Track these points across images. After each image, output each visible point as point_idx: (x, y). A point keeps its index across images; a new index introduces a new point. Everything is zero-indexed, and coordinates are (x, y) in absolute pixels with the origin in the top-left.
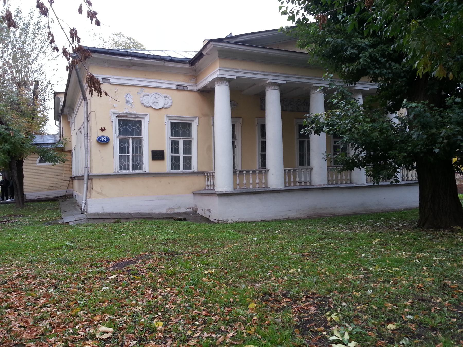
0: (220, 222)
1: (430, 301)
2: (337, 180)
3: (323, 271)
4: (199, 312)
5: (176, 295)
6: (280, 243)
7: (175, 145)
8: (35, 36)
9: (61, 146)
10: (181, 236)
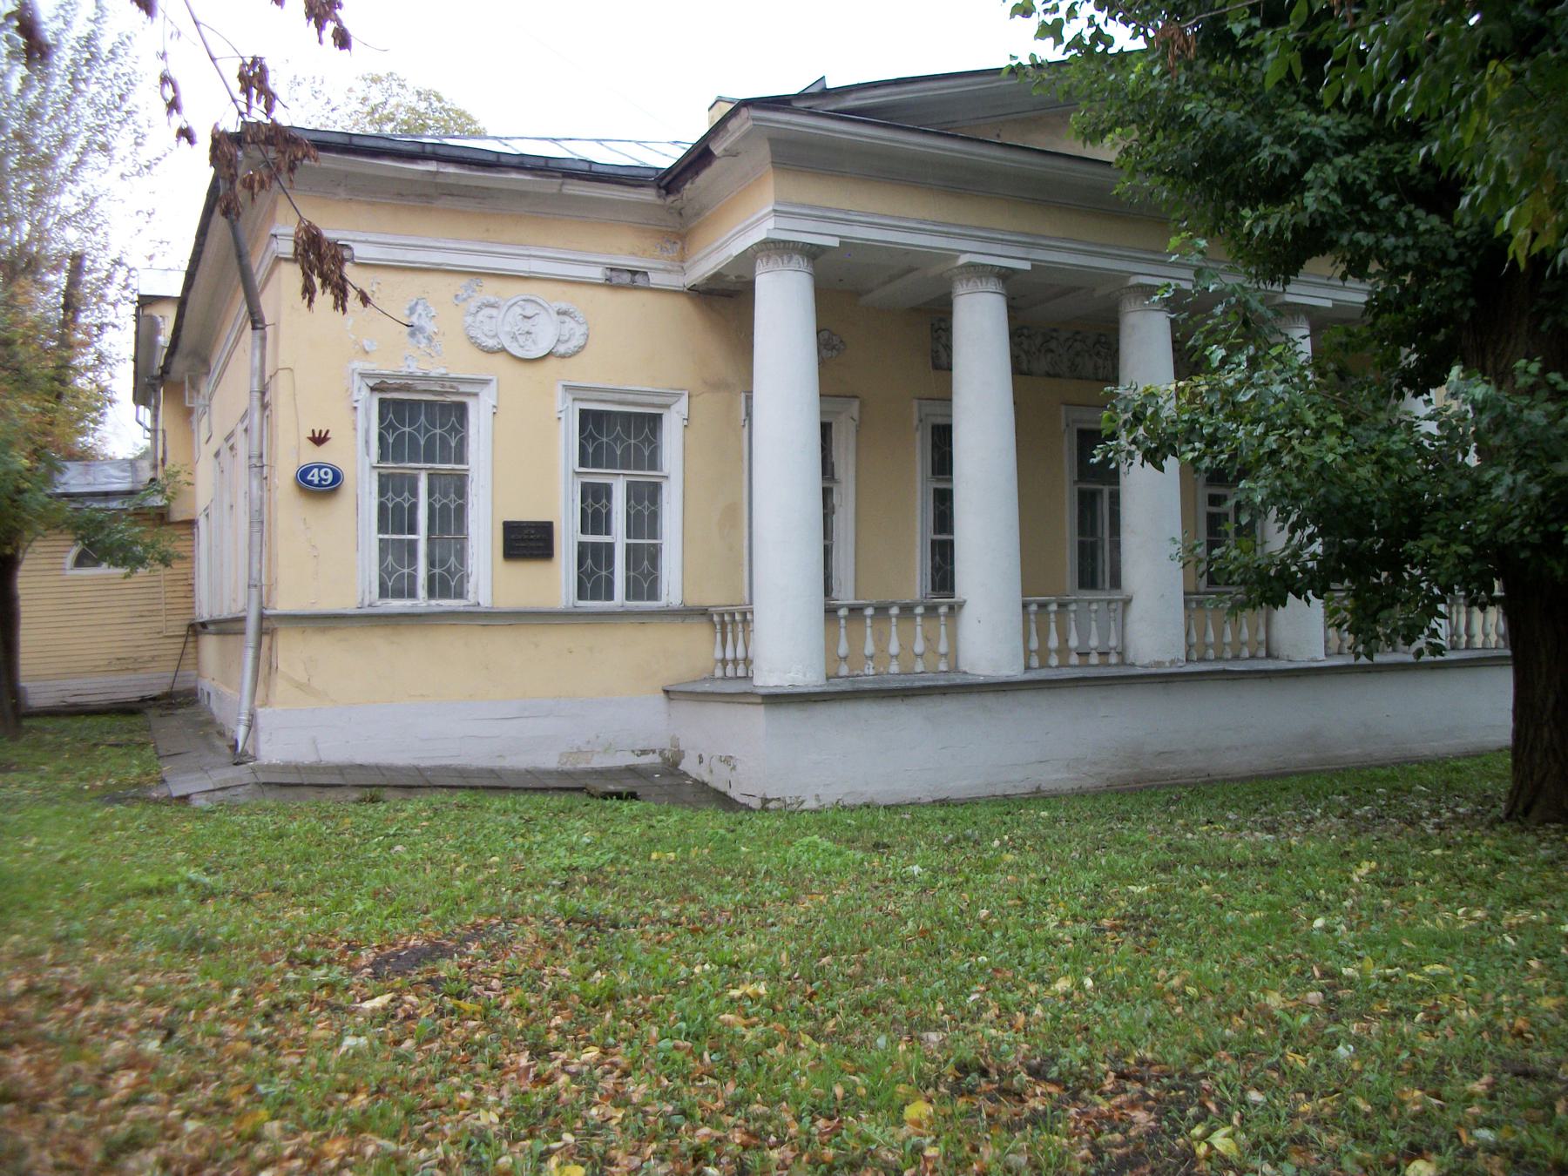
0: (771, 805)
1: (1550, 1077)
2: (1220, 644)
3: (1175, 982)
4: (718, 1134)
5: (626, 1074)
6: (1011, 884)
7: (597, 500)
8: (76, 90)
9: (158, 501)
10: (624, 858)
